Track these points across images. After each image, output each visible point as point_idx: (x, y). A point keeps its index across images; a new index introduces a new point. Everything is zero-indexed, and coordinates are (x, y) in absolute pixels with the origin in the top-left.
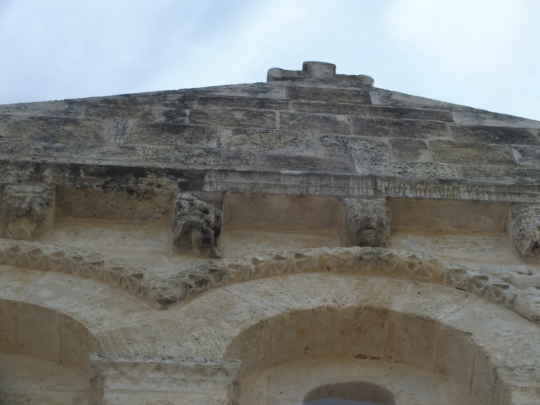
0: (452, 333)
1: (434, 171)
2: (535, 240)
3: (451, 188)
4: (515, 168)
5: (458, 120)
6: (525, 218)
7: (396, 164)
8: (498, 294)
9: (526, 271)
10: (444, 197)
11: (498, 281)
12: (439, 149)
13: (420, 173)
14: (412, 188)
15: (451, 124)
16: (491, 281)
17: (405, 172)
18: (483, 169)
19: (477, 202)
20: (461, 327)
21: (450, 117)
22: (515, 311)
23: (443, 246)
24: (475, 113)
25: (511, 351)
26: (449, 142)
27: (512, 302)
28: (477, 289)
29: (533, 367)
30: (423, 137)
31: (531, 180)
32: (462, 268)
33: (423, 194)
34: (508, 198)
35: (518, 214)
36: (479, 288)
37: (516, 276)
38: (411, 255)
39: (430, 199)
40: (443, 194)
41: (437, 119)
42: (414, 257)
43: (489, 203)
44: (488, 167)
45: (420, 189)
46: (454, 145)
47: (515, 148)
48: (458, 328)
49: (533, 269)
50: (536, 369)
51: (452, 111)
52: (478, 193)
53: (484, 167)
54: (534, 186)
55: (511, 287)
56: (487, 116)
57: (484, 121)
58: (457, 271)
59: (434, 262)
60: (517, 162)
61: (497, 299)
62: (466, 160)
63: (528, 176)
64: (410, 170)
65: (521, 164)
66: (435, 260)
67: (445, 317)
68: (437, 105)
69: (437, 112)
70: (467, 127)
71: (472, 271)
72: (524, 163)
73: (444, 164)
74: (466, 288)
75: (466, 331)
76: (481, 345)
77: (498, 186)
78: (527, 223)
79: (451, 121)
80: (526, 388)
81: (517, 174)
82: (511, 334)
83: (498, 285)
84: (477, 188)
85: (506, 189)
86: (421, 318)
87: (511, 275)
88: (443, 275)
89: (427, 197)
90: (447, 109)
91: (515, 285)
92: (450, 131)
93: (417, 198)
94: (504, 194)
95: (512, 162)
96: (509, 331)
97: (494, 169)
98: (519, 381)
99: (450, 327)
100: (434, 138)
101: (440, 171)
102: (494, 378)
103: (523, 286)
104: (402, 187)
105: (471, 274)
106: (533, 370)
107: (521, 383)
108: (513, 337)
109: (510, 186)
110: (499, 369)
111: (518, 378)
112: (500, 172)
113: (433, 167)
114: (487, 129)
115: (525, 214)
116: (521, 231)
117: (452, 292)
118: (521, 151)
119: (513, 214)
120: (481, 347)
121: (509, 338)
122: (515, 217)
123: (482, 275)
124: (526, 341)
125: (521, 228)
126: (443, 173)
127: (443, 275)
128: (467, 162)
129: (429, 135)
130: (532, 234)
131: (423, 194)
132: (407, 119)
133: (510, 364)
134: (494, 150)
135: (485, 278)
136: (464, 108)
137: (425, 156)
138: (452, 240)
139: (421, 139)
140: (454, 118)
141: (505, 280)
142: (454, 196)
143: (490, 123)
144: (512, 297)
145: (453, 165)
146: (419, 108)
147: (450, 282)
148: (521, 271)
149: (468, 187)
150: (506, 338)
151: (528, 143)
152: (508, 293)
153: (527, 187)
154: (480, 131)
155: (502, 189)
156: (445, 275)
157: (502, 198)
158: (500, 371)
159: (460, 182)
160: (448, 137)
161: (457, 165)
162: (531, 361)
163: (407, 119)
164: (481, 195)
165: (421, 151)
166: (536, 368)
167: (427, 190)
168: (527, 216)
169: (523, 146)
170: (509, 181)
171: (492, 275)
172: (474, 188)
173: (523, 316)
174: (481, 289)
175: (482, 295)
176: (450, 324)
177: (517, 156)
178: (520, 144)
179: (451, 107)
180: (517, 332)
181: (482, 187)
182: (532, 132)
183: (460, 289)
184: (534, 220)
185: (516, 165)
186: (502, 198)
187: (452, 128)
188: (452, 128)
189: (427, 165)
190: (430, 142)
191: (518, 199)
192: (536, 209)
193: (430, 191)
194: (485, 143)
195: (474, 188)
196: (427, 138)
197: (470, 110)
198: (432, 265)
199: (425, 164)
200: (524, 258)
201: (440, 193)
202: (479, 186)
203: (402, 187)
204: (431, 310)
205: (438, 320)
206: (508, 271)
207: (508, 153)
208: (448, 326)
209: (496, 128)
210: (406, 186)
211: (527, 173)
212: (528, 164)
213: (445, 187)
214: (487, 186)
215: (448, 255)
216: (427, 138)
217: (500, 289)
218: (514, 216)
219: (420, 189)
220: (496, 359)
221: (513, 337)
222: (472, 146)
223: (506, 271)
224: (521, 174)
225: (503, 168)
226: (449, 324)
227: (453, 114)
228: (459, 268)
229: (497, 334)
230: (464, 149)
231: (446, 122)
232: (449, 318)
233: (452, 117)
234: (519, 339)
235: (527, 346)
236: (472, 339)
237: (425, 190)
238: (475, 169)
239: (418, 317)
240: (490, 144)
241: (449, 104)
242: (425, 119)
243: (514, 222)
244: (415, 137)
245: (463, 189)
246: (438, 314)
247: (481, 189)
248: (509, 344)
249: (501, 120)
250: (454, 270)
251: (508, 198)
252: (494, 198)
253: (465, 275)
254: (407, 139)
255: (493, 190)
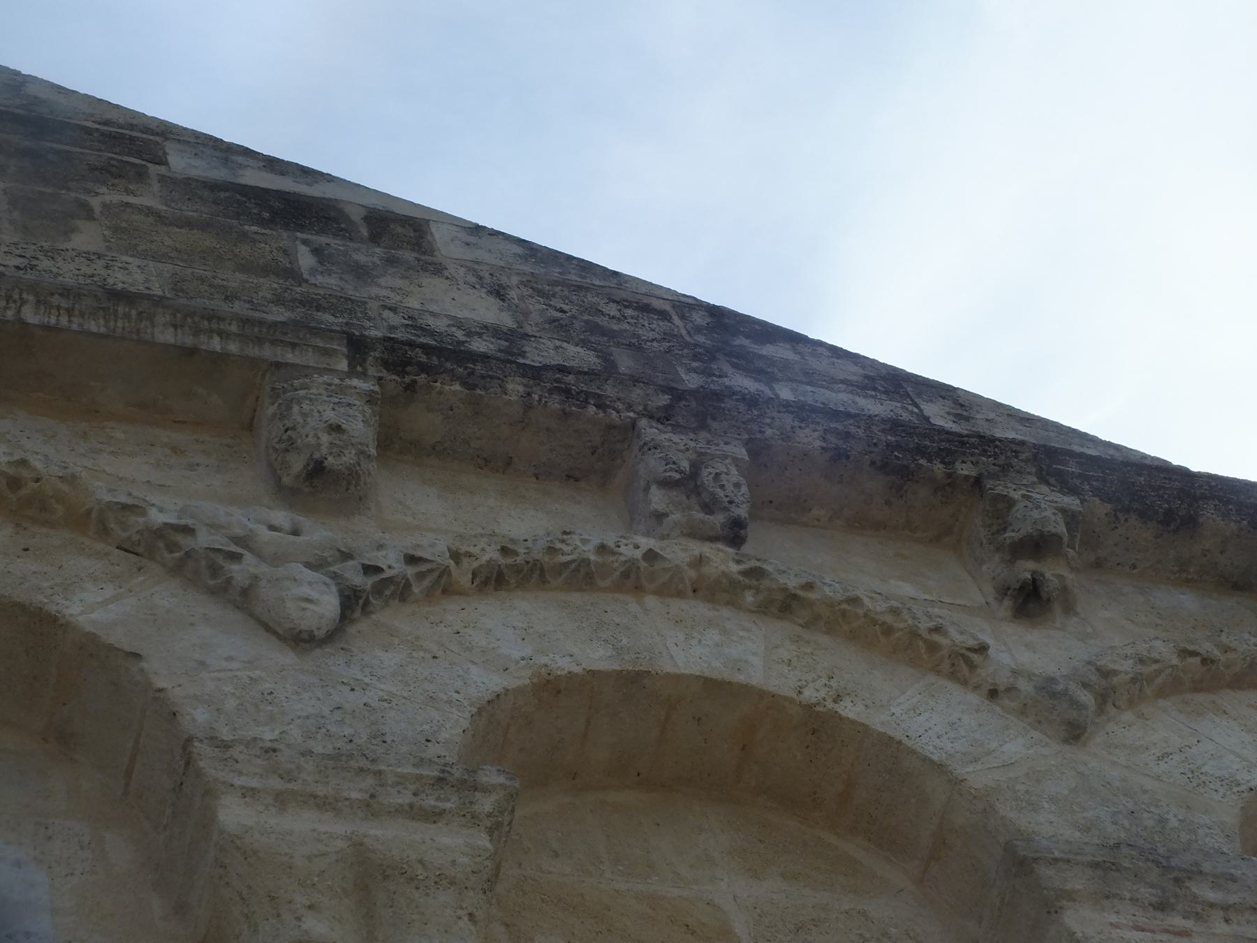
0: (96, 653)
1: (103, 272)
2: (317, 456)
3: (134, 312)
4: (298, 289)
5: (179, 162)
6: (299, 403)
7: (13, 247)
8: (215, 570)
9: (287, 525)
10: (114, 330)
11: (219, 541)
12: (124, 225)
13: (69, 272)
14: (39, 302)
15: (162, 170)
16: (204, 539)
17: (33, 267)
18: (221, 283)
19: (192, 352)
20: (119, 638)
21: (160, 153)
22: (251, 615)
23: (99, 446)
24: (221, 150)
25: (231, 704)
26: (149, 211)
27: (245, 592)
28: (167, 556)
29: (275, 745)
30: (88, 191)
31: (331, 319)
32: (136, 502)
33: (64, 320)
34: (268, 352)
35: (285, 391)
36: (171, 552)
37: (264, 534)
38: (16, 457)
39: (81, 332)
40: (112, 324)
41: (130, 155)
42: (23, 463)
43: (220, 359)
44: (234, 280)
45: (58, 308)
46: (158, 216)
47: (305, 242)
48: (112, 640)
49: (305, 522)
50: (281, 751)
51: (167, 139)
52: (197, 332)
53: (224, 277)
54: (332, 331)
55: (248, 556)
56: (250, 162)
57: (241, 172)
58: (125, 507)
59: (72, 480)
60: (305, 276)
61: (211, 582)
62: (185, 257)
63: (324, 310)
64: (45, 263)
65: (312, 280)
66: (74, 476)
67: (82, 613)
68: (134, 122)
69: (132, 139)
70: (198, 181)
71: (161, 510)
72: (320, 279)
73: (130, 260)
74: (140, 550)
75: (128, 649)
76: (161, 683)
77: (245, 322)
78: (304, 415)
79: (163, 162)
80: (253, 789)
81: (301, 302)
82: (234, 665)
83: (219, 550)
84: (196, 319)
85: (265, 330)
86: (23, 607)
87: (251, 530)
88: (89, 512)
89: (75, 327)
90: (157, 134)
91: (258, 555)
92: (156, 187)
93: (47, 328)
94: (259, 341)
95: (292, 274)
96: (230, 659)
97: (247, 285)
98: (240, 773)
99: (93, 638)
100: (114, 197)
101: (119, 275)
102: (183, 763)
103: (277, 559)
104: (16, 296)
105: (157, 518)
106: (274, 750)
107: (243, 778)
108: (238, 673)
109: (274, 325)
110: (196, 744)
111: (238, 766)
112: (261, 294)
113: (102, 262)
114: (246, 191)
115: (302, 392)
116: (286, 430)
117: (107, 554)
118: (317, 251)
119: (273, 389)
120: (161, 690)
121: (229, 674)
122: (278, 396)
123: (183, 522)
124: (267, 686)
125: (289, 424)
126: (125, 279)
127: (89, 512)
128: (185, 261)
129: (103, 190)
130: (311, 439)
131: (64, 320)
132: (55, 145)
133: (225, 734)
134: (254, 241)
135: (188, 531)
136: (197, 137)
137: (87, 237)
138: (120, 435)
139: (83, 197)
140: (170, 158)
141: (237, 540)
142: (138, 332)
143: (253, 178)
144: (247, 582)
145: (151, 264)
146: (89, 124)
147: (104, 532)
148: (276, 522)
149: (175, 316)
150: (222, 675)
151: (335, 235)
152: (239, 572)
153: (316, 331)
154: (227, 194)
155: (256, 329)
156: (94, 515)
157: (252, 351)
158: (200, 748)
159: (158, 302)
160: (149, 198)
161: (160, 265)
162: (273, 730)
163: (55, 145)
164: (203, 338)
165: (80, 224)
166: (282, 747)
167: (77, 312)
168: (305, 398)
169: (323, 240)
170: (279, 314)
171: (207, 525)
172: (189, 320)
173: (267, 628)
174: (177, 555)
175: (177, 570)
176: (92, 630)
177: (305, 260)
178: (317, 233)
179: (168, 132)
180: (249, 662)
181: (209, 319)
182: (348, 209)
183: (126, 551)
184: (320, 408)
185: (301, 280)
186: (252, 351)
187: (162, 179)
188: (162, 179)
189: (89, 256)
190: (104, 205)
191: (290, 357)
192: (329, 385)
193: (82, 315)
194: (235, 222)
195: (189, 320)
196: (97, 194)
197: (211, 144)
198: (65, 487)
199: (82, 256)
200: (287, 495)
201: (107, 321)
202: (203, 317)
203: (16, 296)
204: (49, 592)
205: (64, 616)
206: (245, 521)
207: (285, 252)
208: (88, 633)
209: (266, 191)
210: (25, 296)
211: (325, 305)
212: (330, 282)
213: (121, 310)
214: (220, 319)
215: (107, 469)
216: (97, 194)
217: (220, 560)
218: (275, 394)
219: (58, 308)
220: (194, 720)
221: (238, 673)
222: (204, 226)
223: (238, 519)
224: (309, 302)
225: (269, 285)
226: (89, 628)
227: (170, 147)
228: (129, 501)
229: (202, 664)
230: (183, 231)
231: (149, 165)
232: (93, 616)
233: (165, 154)
234: (252, 679)
235: (269, 697)
236: (142, 670)
237: (70, 312)
238: (202, 280)
239: (15, 604)
240: (246, 227)
241: (1117, 448)
242: (99, 150)
243: (272, 410)
244: (69, 189)
245: (162, 318)
246: (67, 603)
247: (206, 323)
248: (229, 688)
249: (283, 174)
250: (117, 503)
251: (268, 352)
252: (233, 347)
253: (141, 520)
254: (49, 190)
255: (234, 328)
